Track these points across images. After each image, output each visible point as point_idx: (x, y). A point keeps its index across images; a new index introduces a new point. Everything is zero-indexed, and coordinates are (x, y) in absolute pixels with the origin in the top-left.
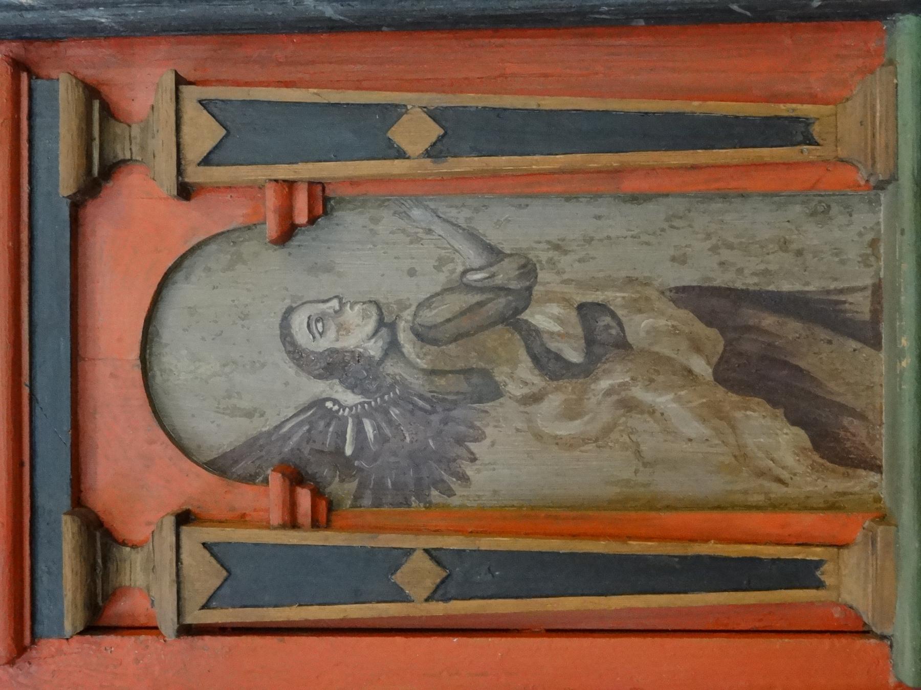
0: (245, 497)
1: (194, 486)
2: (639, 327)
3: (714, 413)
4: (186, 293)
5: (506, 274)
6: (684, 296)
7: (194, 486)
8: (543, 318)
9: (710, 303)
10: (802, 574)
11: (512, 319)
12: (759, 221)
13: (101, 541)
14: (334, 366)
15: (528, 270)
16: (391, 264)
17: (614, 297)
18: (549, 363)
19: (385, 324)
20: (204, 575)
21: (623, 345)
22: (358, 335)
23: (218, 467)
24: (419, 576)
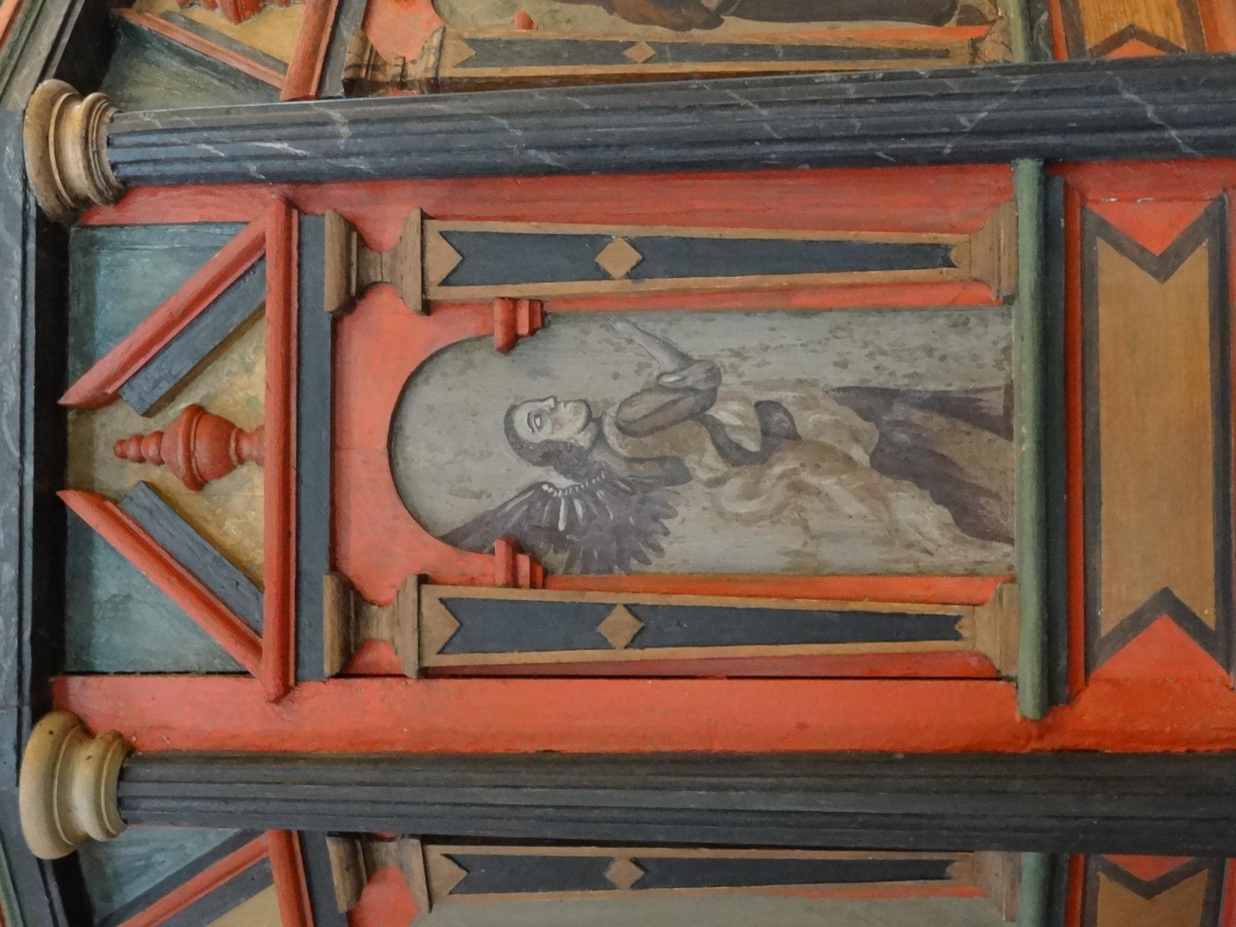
0: (475, 564)
1: (432, 555)
2: (807, 422)
3: (870, 494)
4: (426, 394)
5: (695, 376)
6: (845, 394)
7: (432, 555)
8: (725, 413)
9: (870, 401)
10: (944, 627)
11: (700, 416)
12: (907, 331)
13: (354, 603)
14: (550, 455)
15: (714, 374)
16: (596, 369)
17: (787, 396)
18: (732, 453)
19: (593, 420)
20: (440, 626)
21: (794, 437)
22: (570, 428)
23: (452, 539)
24: (619, 626)
